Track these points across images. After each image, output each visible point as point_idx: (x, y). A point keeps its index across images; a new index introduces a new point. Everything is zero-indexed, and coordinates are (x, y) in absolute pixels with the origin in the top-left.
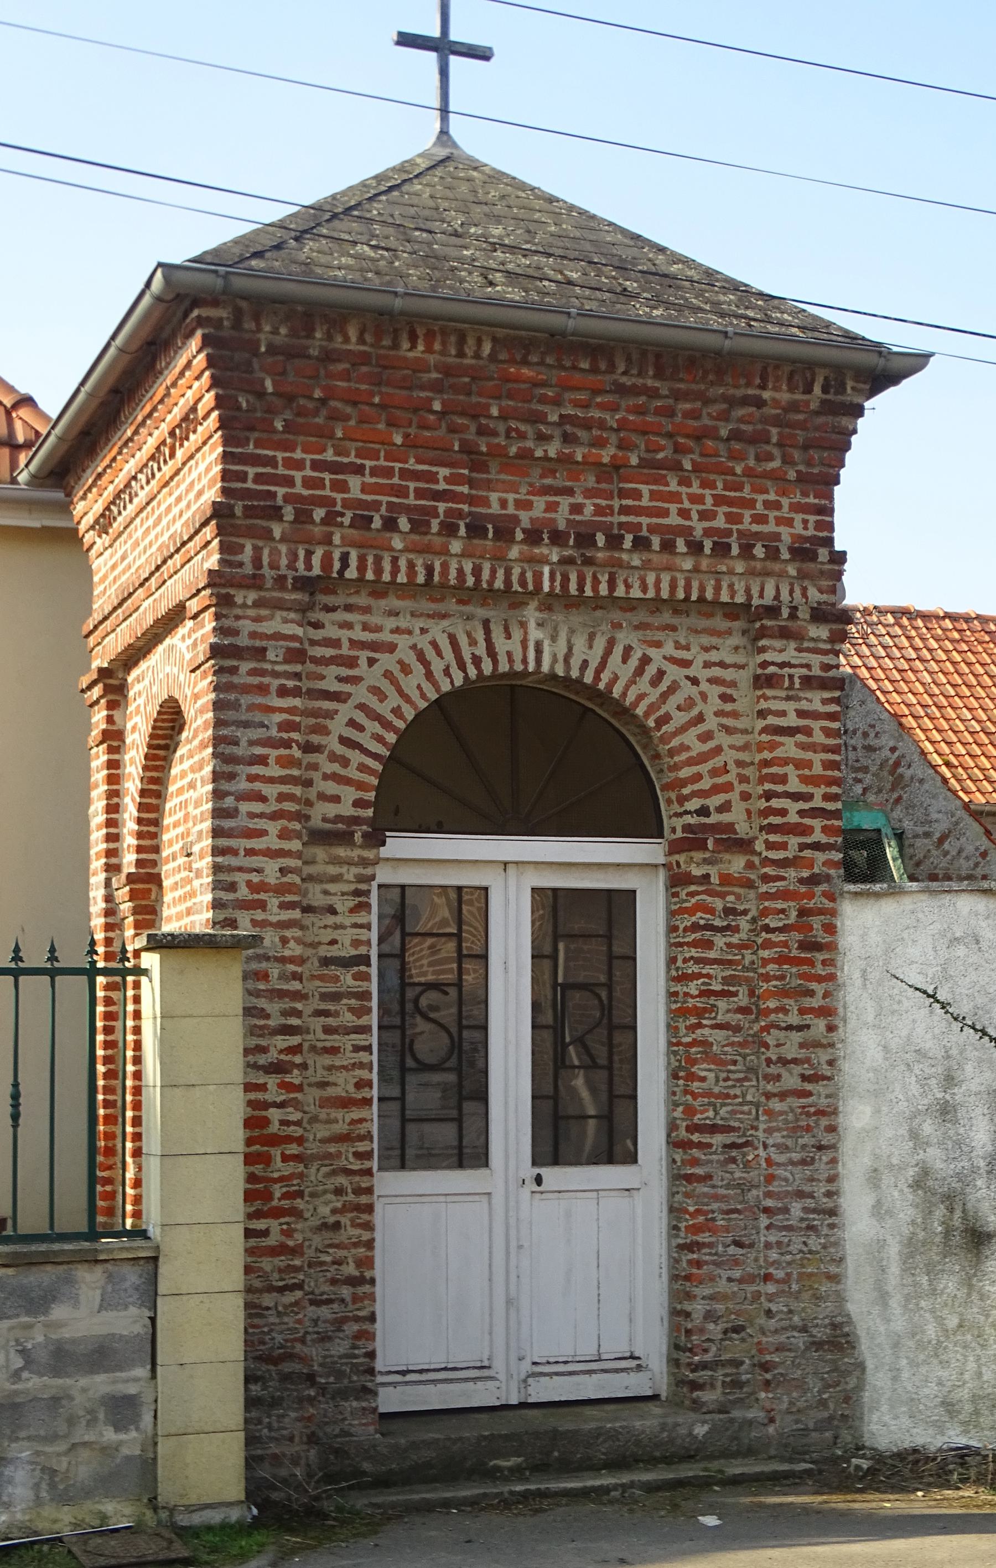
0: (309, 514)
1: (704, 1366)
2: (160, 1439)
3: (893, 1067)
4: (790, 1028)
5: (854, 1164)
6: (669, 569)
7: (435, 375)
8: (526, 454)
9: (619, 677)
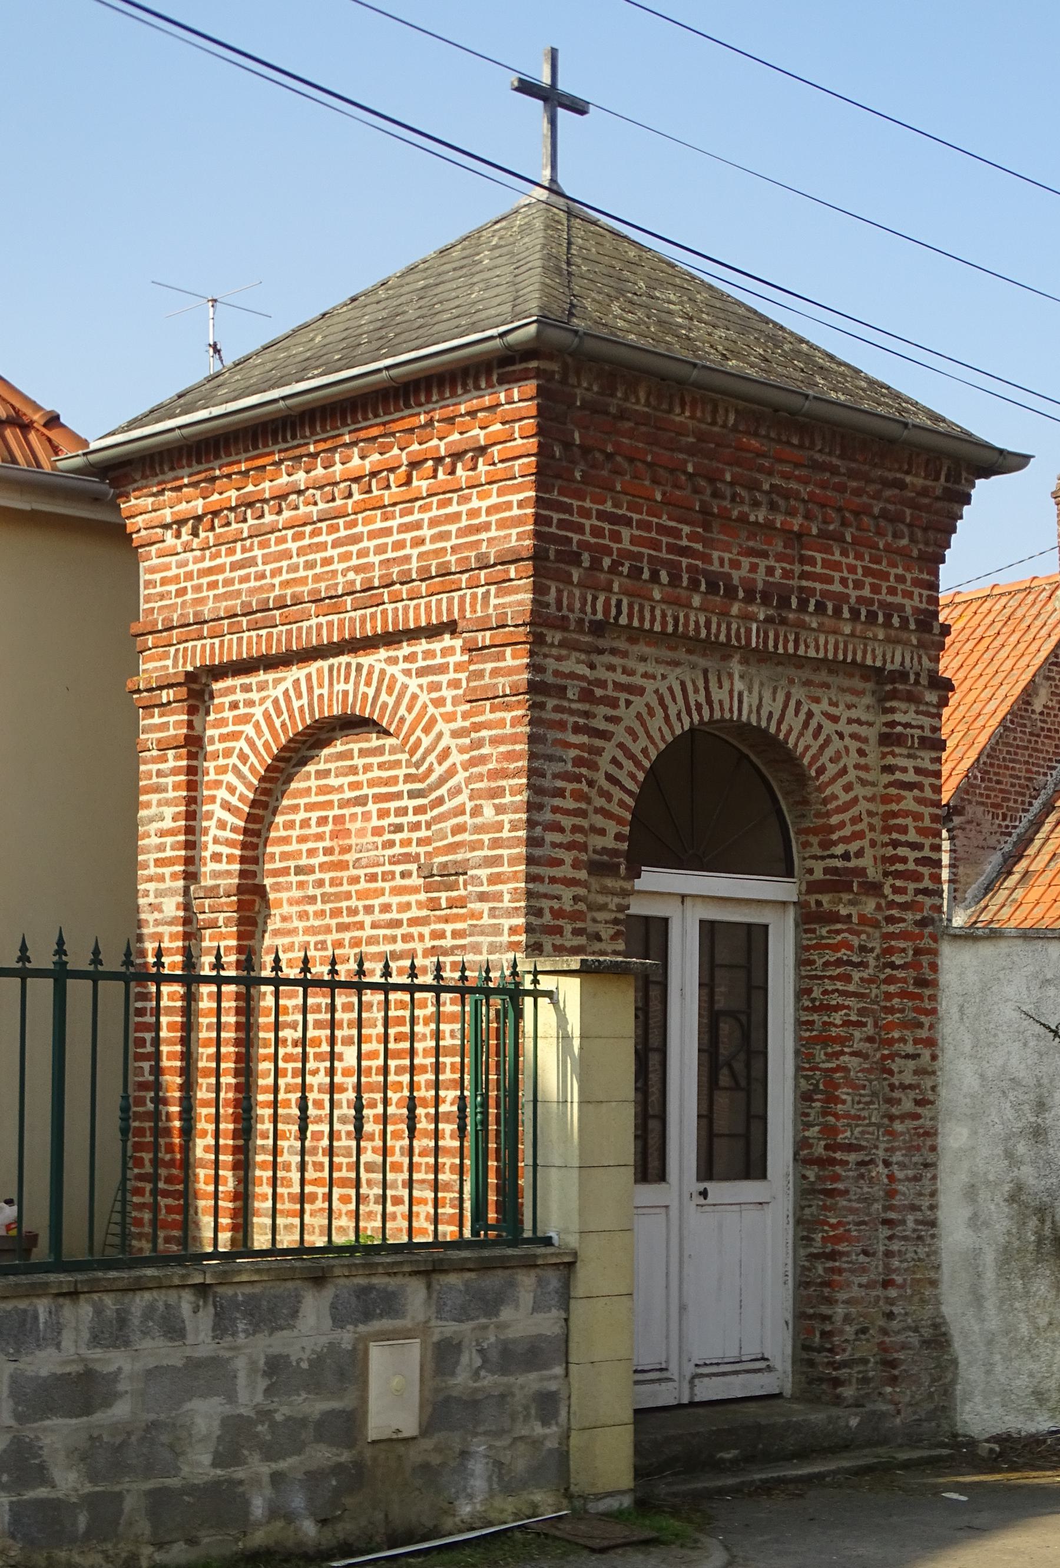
0: (600, 561)
1: (844, 1364)
2: (573, 1433)
3: (989, 1093)
4: (907, 1056)
5: (951, 1182)
6: (835, 632)
7: (691, 440)
8: (743, 519)
9: (792, 732)
